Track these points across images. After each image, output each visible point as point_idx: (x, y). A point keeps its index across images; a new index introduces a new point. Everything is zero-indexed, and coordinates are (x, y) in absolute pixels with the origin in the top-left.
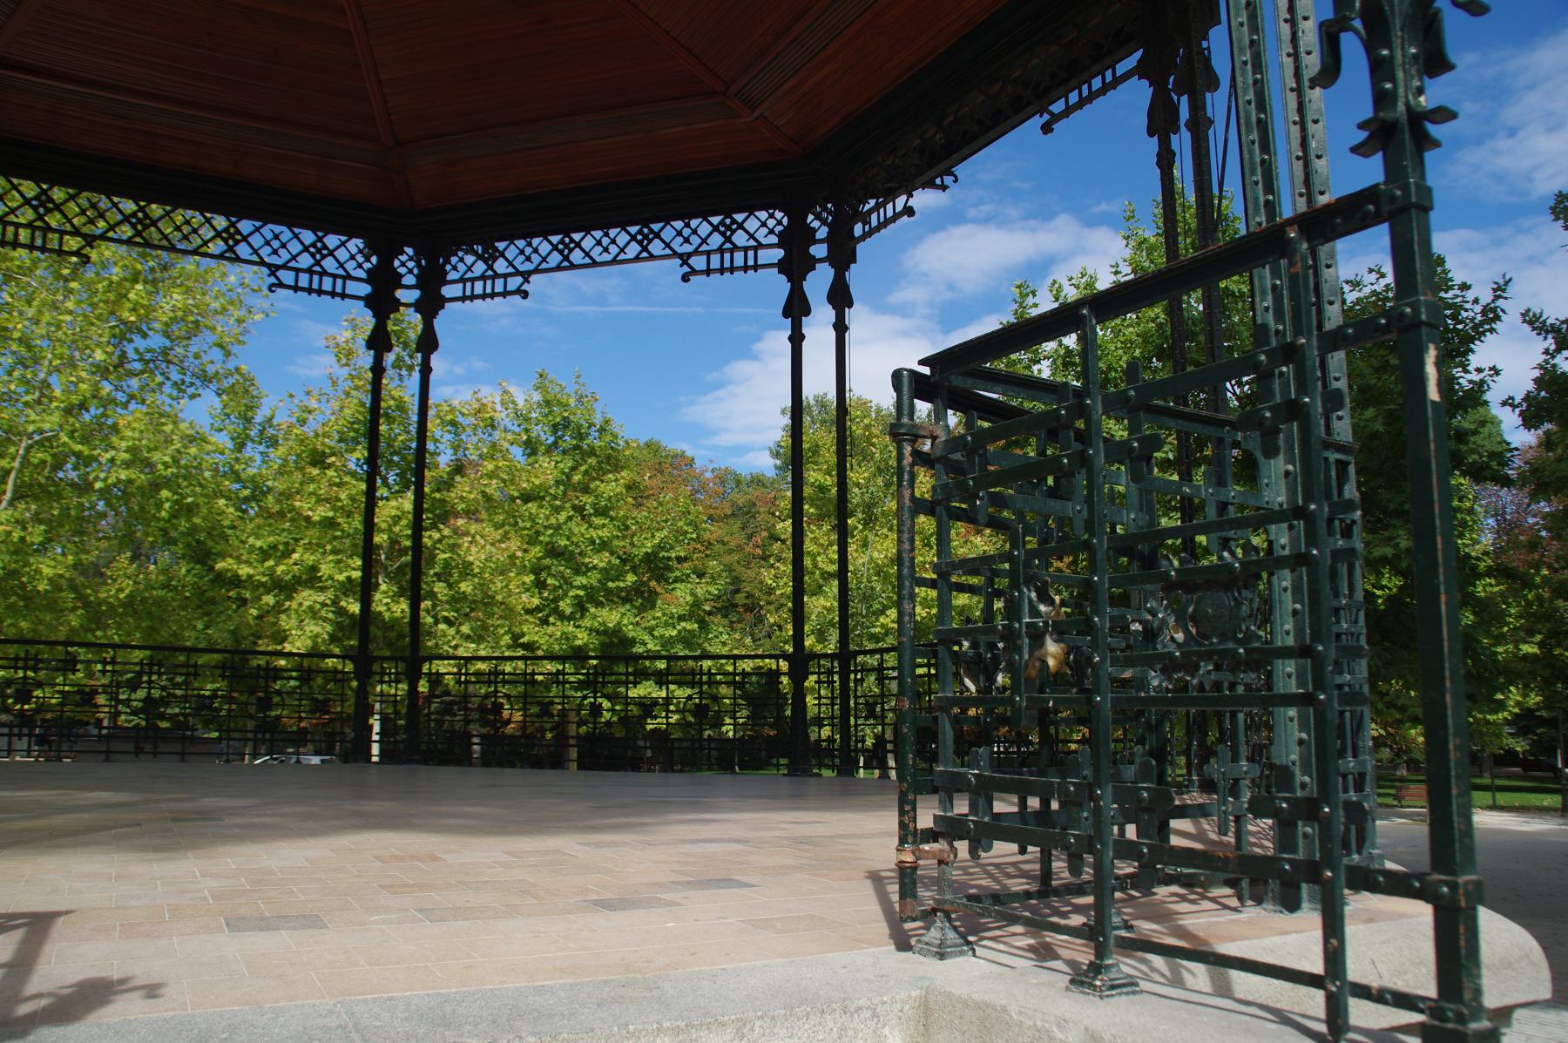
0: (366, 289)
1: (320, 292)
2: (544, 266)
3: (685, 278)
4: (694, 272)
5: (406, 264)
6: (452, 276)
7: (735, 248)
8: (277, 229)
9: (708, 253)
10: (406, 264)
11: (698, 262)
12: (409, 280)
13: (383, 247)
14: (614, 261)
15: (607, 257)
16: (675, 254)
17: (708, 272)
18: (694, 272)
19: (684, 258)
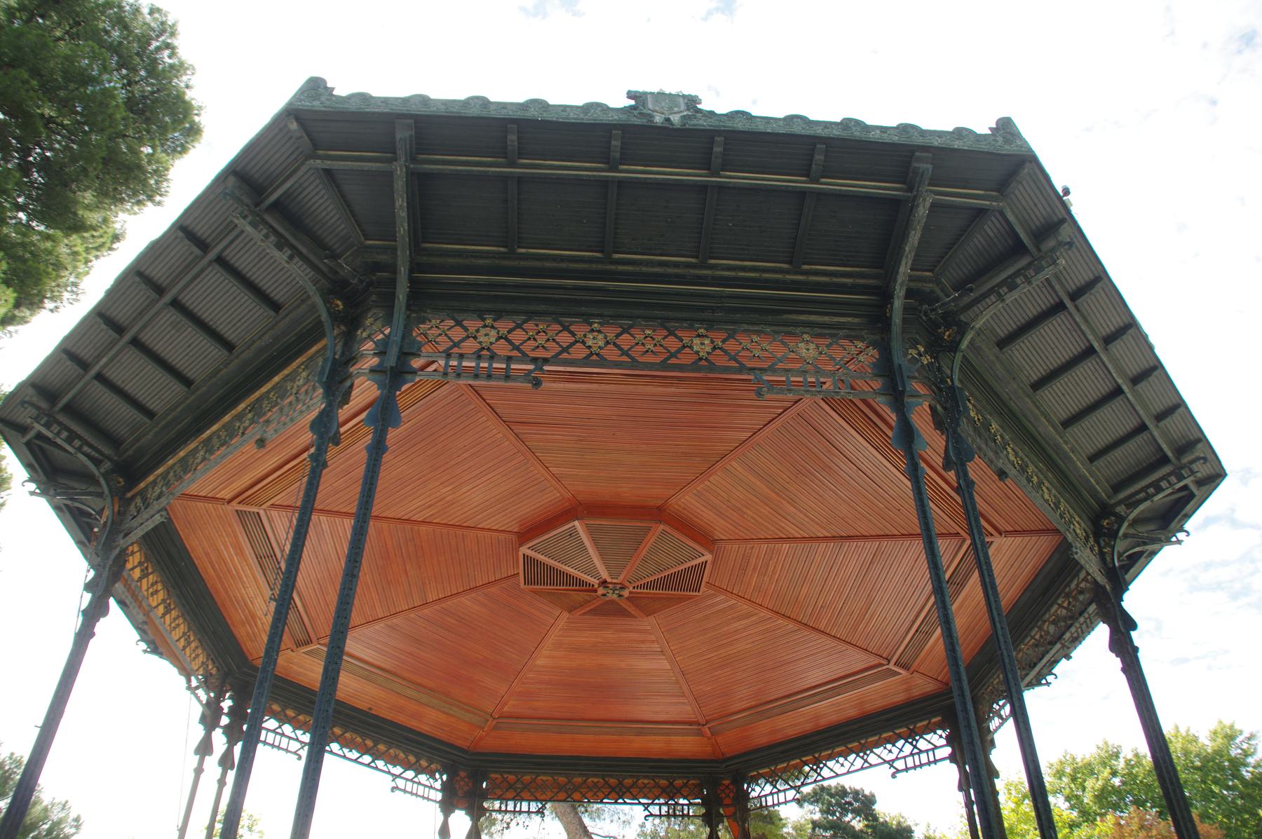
0: (948, 750)
1: (921, 765)
2: (853, 768)
3: (894, 776)
4: (898, 771)
7: (921, 751)
8: (398, 752)
9: (904, 757)
11: (900, 764)
14: (848, 772)
15: (844, 770)
16: (885, 762)
17: (907, 769)
18: (898, 771)
19: (891, 763)
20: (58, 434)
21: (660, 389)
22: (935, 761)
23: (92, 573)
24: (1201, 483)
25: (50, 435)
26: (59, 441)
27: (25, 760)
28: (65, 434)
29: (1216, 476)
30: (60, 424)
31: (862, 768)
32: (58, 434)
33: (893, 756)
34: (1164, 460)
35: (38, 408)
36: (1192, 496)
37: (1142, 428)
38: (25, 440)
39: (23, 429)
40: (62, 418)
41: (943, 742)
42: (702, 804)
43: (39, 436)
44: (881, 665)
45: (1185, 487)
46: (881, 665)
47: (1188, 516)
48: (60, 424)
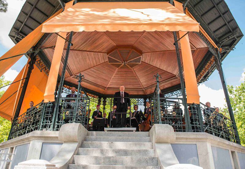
5: (102, 99)
6: (107, 102)
10: (102, 99)
12: (102, 101)
13: (145, 99)
20: (20, 36)
21: (69, 98)
22: (141, 105)
23: (30, 60)
24: (237, 37)
25: (19, 37)
26: (20, 38)
27: (10, 69)
28: (21, 37)
29: (241, 36)
30: (20, 35)
31: (172, 96)
32: (20, 36)
33: (177, 94)
34: (230, 32)
35: (15, 32)
36: (236, 40)
37: (225, 24)
38: (15, 39)
39: (14, 37)
40: (20, 34)
41: (143, 102)
42: (144, 103)
43: (17, 38)
44: (142, 88)
45: (234, 38)
46: (142, 88)
47: (235, 45)
48: (20, 35)
